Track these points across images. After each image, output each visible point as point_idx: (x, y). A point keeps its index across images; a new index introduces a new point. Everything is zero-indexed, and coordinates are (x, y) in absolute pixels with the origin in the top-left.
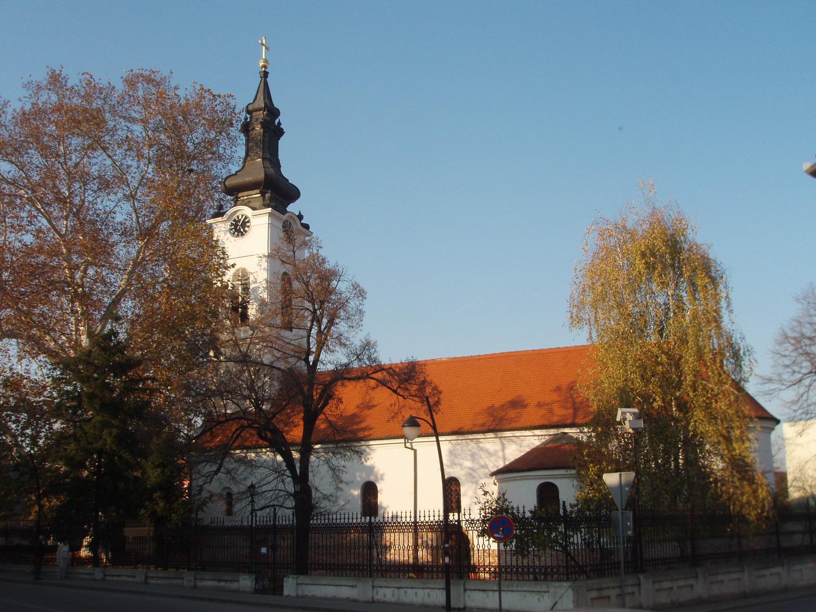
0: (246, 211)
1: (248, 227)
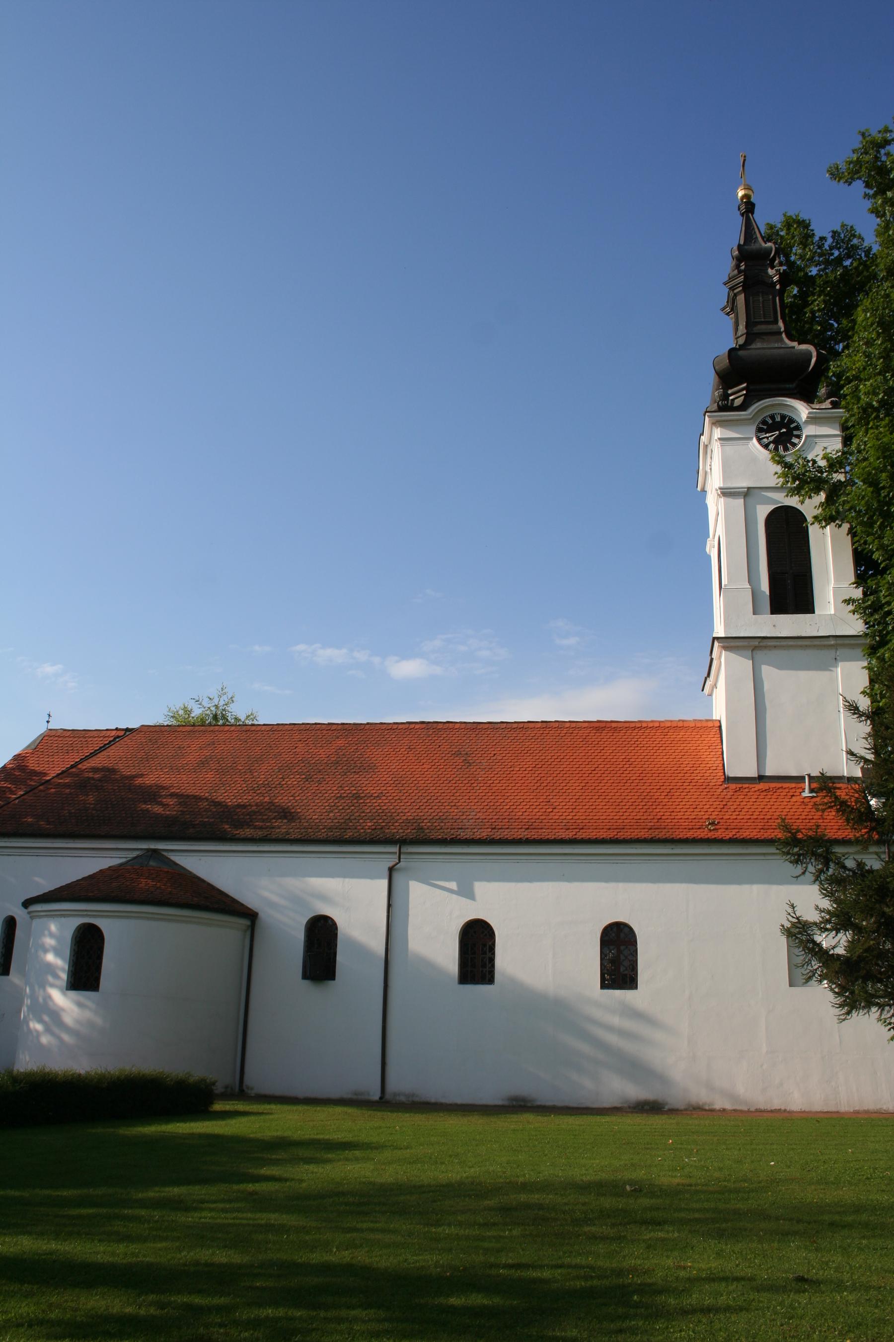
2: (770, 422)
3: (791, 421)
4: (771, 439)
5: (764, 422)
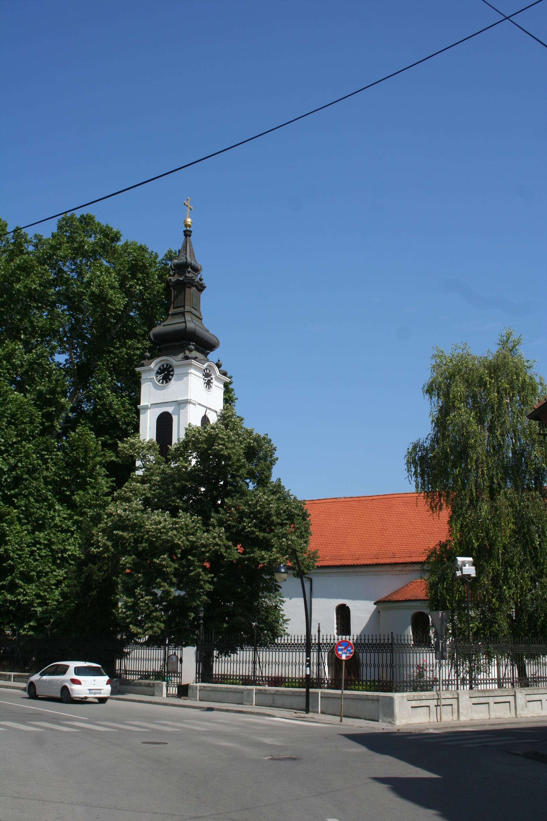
0: (173, 360)
1: (172, 375)
2: (171, 373)
3: (171, 367)
4: (161, 378)
5: (160, 369)
